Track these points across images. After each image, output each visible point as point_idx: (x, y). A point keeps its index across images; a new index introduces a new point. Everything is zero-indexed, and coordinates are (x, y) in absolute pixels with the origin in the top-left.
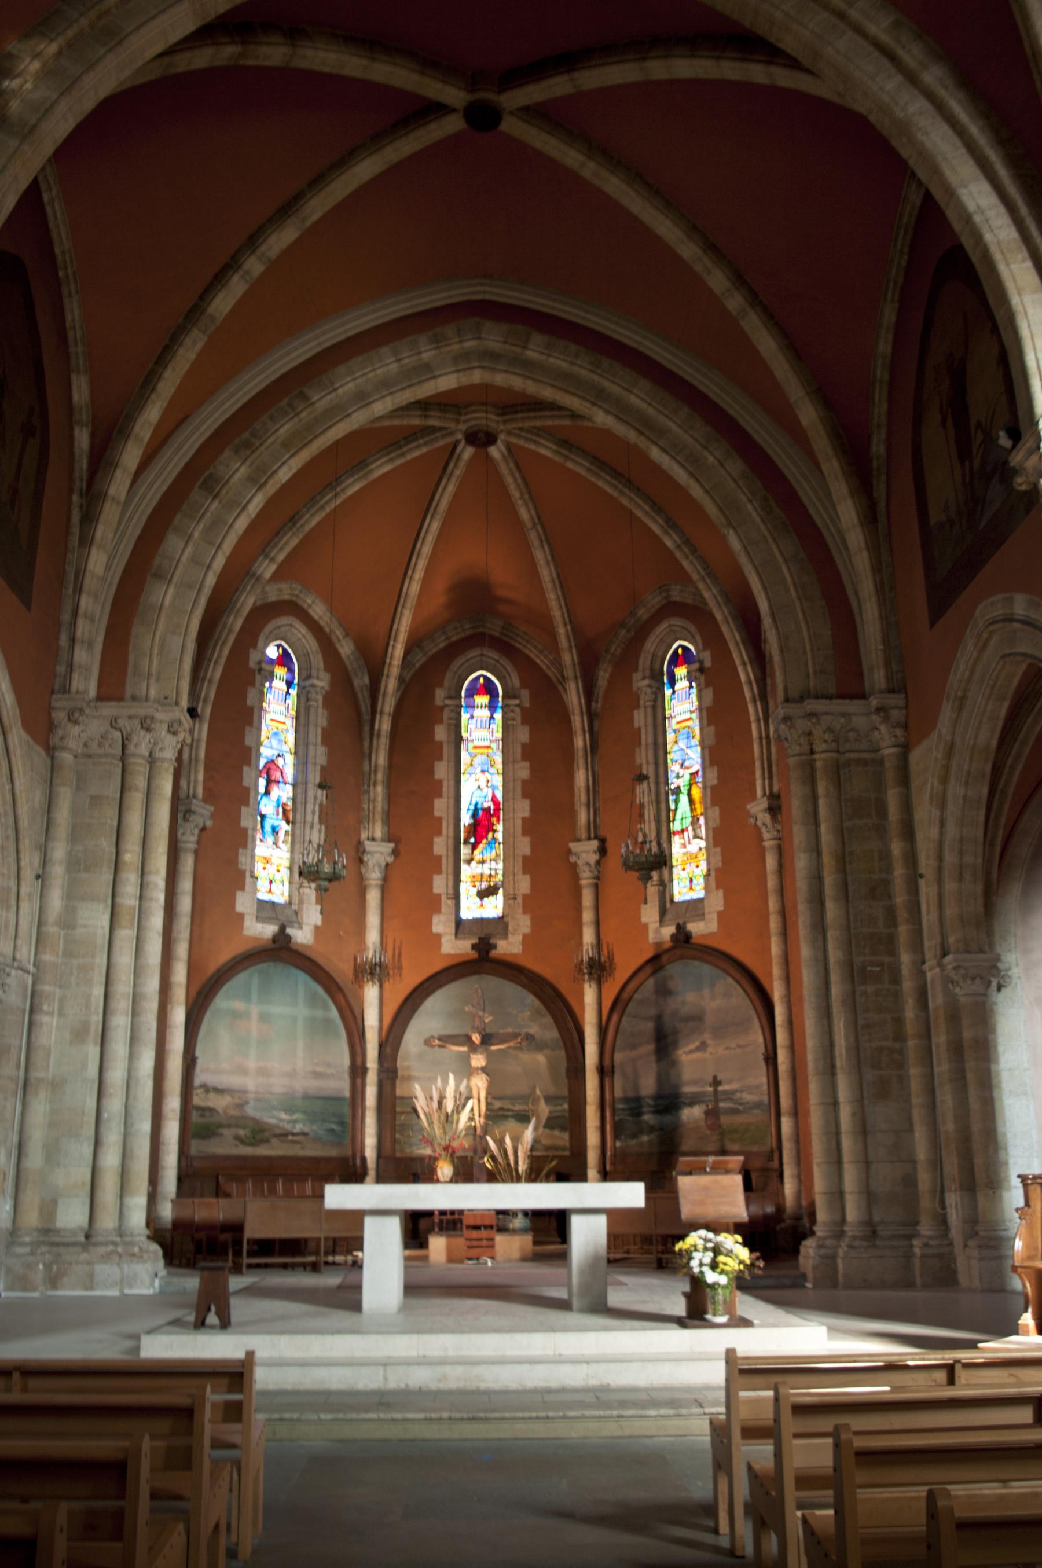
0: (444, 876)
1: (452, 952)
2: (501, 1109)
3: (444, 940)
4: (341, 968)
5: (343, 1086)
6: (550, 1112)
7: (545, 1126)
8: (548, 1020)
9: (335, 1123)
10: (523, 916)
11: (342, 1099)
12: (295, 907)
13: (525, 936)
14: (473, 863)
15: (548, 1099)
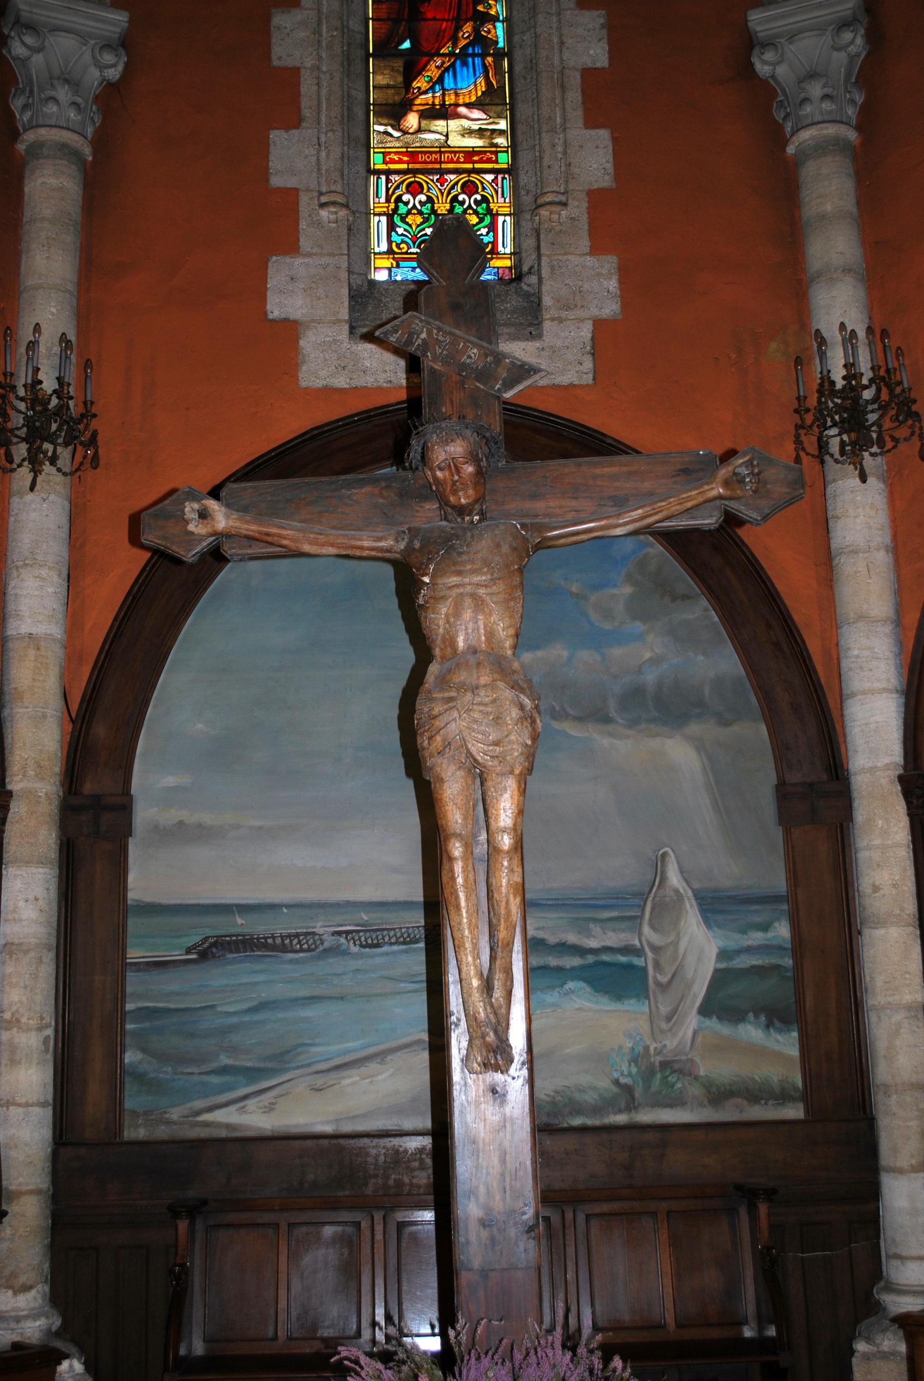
0: (307, 132)
1: (341, 382)
3: (308, 343)
6: (723, 954)
7: (705, 1011)
8: (701, 612)
10: (590, 261)
13: (598, 324)
14: (412, 120)
15: (715, 905)
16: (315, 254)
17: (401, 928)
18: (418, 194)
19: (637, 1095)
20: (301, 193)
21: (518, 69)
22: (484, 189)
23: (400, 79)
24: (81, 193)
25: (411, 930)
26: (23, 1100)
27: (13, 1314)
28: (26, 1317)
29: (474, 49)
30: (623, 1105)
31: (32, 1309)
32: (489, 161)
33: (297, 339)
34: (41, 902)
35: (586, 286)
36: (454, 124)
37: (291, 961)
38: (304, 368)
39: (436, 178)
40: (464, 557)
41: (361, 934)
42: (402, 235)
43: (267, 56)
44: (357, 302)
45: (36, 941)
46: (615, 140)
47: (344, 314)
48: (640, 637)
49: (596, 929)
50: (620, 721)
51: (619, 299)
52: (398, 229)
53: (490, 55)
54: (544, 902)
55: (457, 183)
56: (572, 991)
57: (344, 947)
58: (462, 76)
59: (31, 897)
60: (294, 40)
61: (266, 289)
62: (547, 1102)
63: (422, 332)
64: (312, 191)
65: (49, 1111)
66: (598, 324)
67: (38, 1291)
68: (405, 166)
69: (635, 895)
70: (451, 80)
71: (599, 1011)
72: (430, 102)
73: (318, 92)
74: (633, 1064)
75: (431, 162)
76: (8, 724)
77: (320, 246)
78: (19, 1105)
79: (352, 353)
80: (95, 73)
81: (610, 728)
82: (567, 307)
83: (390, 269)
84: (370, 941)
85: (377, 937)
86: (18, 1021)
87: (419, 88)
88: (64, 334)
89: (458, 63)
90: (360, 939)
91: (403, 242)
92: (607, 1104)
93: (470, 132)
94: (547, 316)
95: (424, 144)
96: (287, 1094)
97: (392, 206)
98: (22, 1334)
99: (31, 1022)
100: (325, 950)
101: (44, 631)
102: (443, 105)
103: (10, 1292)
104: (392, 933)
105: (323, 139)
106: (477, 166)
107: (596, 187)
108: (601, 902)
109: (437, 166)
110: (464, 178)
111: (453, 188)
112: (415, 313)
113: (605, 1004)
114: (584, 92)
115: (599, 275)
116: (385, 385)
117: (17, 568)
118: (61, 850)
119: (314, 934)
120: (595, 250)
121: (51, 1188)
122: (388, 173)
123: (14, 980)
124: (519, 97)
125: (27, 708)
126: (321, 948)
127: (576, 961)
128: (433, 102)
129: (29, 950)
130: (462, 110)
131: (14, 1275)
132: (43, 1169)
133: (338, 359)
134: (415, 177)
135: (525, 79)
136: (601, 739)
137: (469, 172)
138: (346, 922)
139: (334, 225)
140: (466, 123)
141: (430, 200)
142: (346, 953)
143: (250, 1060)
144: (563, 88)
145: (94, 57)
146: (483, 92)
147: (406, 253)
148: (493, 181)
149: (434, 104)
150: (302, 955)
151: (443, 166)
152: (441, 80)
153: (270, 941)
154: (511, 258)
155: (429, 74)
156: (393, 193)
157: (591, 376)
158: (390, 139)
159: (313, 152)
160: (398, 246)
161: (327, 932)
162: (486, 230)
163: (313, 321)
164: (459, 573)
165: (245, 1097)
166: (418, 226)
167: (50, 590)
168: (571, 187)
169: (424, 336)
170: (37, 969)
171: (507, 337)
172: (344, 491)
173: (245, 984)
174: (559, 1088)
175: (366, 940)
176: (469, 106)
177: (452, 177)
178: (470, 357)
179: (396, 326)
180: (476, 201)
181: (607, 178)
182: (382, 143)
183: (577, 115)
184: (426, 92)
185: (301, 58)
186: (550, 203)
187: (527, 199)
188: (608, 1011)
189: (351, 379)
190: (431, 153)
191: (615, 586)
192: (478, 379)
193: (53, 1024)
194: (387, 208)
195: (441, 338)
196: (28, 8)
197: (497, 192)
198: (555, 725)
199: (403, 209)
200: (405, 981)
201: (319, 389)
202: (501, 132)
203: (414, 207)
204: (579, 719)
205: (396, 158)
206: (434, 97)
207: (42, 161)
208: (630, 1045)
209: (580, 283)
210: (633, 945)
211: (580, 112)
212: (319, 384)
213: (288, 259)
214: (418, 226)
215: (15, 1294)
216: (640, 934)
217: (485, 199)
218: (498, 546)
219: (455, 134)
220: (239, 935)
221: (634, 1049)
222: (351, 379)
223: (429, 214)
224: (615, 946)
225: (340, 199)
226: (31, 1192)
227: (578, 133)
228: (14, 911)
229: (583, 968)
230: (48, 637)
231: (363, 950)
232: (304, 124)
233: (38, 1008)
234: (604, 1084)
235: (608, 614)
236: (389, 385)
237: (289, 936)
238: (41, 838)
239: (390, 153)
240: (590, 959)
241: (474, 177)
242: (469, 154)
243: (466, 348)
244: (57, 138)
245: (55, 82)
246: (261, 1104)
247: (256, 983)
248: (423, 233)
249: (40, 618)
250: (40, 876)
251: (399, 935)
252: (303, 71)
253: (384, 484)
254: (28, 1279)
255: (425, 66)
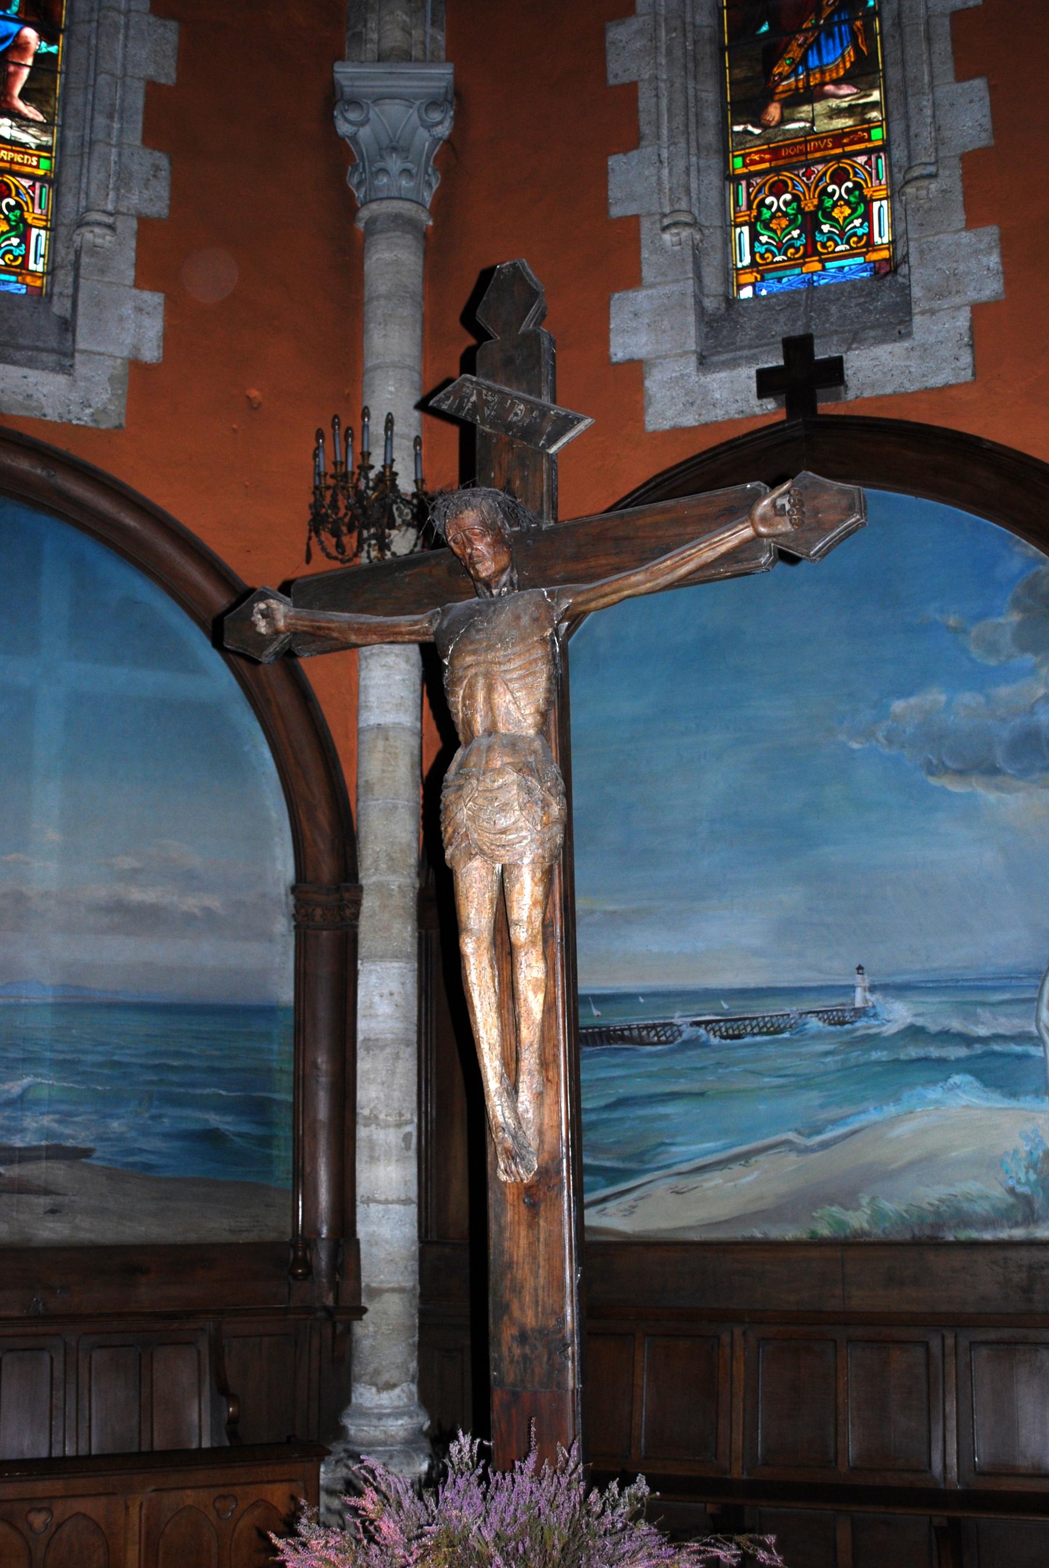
0: (647, 150)
1: (690, 420)
2: (914, 1033)
3: (654, 383)
4: (263, 536)
5: (267, 962)
9: (224, 1107)
10: (966, 237)
11: (268, 1011)
12: (60, 307)
13: (977, 309)
14: (774, 112)
16: (659, 284)
17: (764, 1017)
18: (784, 193)
19: (1036, 1206)
20: (642, 219)
21: (886, 28)
22: (856, 174)
23: (759, 68)
24: (421, 262)
25: (774, 1020)
26: (383, 1198)
27: (376, 1411)
28: (389, 1415)
29: (840, 17)
30: (1020, 1218)
31: (398, 1407)
32: (862, 140)
33: (641, 381)
34: (396, 997)
35: (962, 267)
36: (819, 107)
37: (650, 1055)
38: (650, 411)
39: (801, 172)
40: (482, 635)
41: (722, 1024)
42: (767, 243)
43: (603, 76)
44: (712, 327)
45: (393, 1036)
46: (992, 89)
47: (692, 345)
48: (1033, 671)
49: (984, 1013)
50: (1010, 771)
51: (1001, 276)
52: (761, 238)
53: (857, 19)
54: (923, 985)
55: (825, 174)
56: (957, 1086)
57: (703, 1039)
58: (827, 49)
59: (386, 992)
60: (631, 53)
61: (607, 330)
62: (930, 1212)
63: (472, 395)
64: (653, 214)
65: (413, 1210)
66: (977, 309)
67: (403, 1391)
68: (767, 165)
69: (1031, 974)
70: (816, 57)
71: (990, 1109)
72: (793, 87)
73: (657, 105)
74: (1031, 1171)
75: (796, 155)
76: (362, 818)
77: (664, 274)
78: (379, 1202)
79: (700, 386)
80: (422, 132)
81: (999, 779)
82: (941, 295)
83: (753, 285)
84: (731, 1032)
85: (738, 1028)
86: (376, 1117)
87: (780, 74)
88: (390, 414)
89: (823, 36)
90: (720, 1029)
91: (767, 251)
92: (1002, 1217)
93: (838, 113)
94: (916, 310)
95: (788, 136)
96: (649, 1196)
97: (754, 213)
98: (385, 1432)
99: (389, 1118)
100: (685, 1043)
101: (392, 721)
102: (807, 86)
103: (374, 1390)
104: (754, 1023)
105: (665, 154)
106: (848, 149)
107: (970, 149)
108: (989, 983)
109: (803, 158)
110: (833, 166)
111: (821, 179)
112: (468, 376)
113: (997, 1101)
114: (954, 41)
115: (977, 252)
116: (736, 416)
117: (366, 658)
118: (420, 944)
119: (671, 1024)
120: (971, 224)
121: (418, 1287)
122: (749, 177)
123: (372, 1076)
124: (888, 60)
125: (377, 800)
126: (680, 1040)
127: (962, 1052)
128: (797, 86)
129: (386, 1046)
130: (830, 88)
131: (377, 1372)
132: (406, 1268)
133: (686, 395)
134: (778, 175)
135: (893, 37)
136: (987, 794)
137: (838, 158)
138: (705, 1012)
139: (678, 248)
140: (834, 103)
141: (796, 198)
142: (705, 1045)
143: (608, 1159)
144: (929, 40)
145: (420, 117)
146: (851, 63)
147: (772, 263)
148: (866, 163)
149: (797, 88)
150: (659, 1047)
151: (810, 157)
152: (804, 60)
153: (626, 1033)
154: (888, 249)
155: (790, 55)
156: (755, 198)
157: (969, 371)
158: (749, 138)
159: (653, 170)
160: (762, 256)
161: (686, 1023)
162: (860, 220)
163: (659, 357)
164: (474, 652)
165: (605, 1200)
166: (783, 230)
167: (398, 678)
168: (941, 155)
169: (474, 398)
170: (393, 1064)
171: (872, 341)
172: (397, 574)
173: (603, 1079)
174: (944, 1197)
175: (727, 1031)
176: (837, 82)
177: (820, 167)
178: (516, 414)
179: (449, 392)
180: (847, 190)
181: (983, 135)
182: (741, 144)
183: (946, 67)
184: (787, 78)
185: (638, 70)
186: (916, 178)
187: (899, 177)
188: (1001, 1109)
189: (700, 415)
190: (795, 145)
191: (1000, 614)
192: (523, 438)
193: (416, 1120)
194: (749, 216)
195: (489, 398)
196: (350, 83)
197: (870, 174)
198: (933, 781)
199: (766, 214)
200: (770, 1076)
201: (668, 431)
202: (874, 105)
203: (779, 209)
204: (961, 773)
205: (756, 157)
206: (797, 81)
207: (376, 237)
208: (1027, 1148)
209: (955, 265)
210: (1029, 1032)
211: (950, 64)
212: (666, 425)
213: (631, 294)
214: (845, 218)
215: (379, 1391)
216: (1038, 1020)
217: (857, 186)
218: (518, 618)
219: (822, 117)
220: (595, 1027)
221: (1031, 1153)
222: (700, 415)
223: (796, 215)
224: (1008, 1033)
225: (685, 218)
226: (393, 1290)
227: (949, 88)
228: (370, 1007)
229: (969, 1058)
230: (397, 726)
231: (723, 1041)
232: (643, 143)
233: (396, 1105)
234: (998, 1192)
235: (992, 648)
236: (740, 416)
237: (646, 1027)
238: (394, 931)
239: (750, 154)
240: (978, 1049)
241: (845, 163)
242: (838, 137)
243: (513, 404)
244: (389, 209)
245: (384, 153)
246: (622, 1207)
247: (612, 1079)
248: (851, 225)
249: (388, 707)
250: (395, 971)
251: (761, 1024)
252: (640, 85)
253: (433, 562)
254: (391, 1377)
255: (787, 46)
